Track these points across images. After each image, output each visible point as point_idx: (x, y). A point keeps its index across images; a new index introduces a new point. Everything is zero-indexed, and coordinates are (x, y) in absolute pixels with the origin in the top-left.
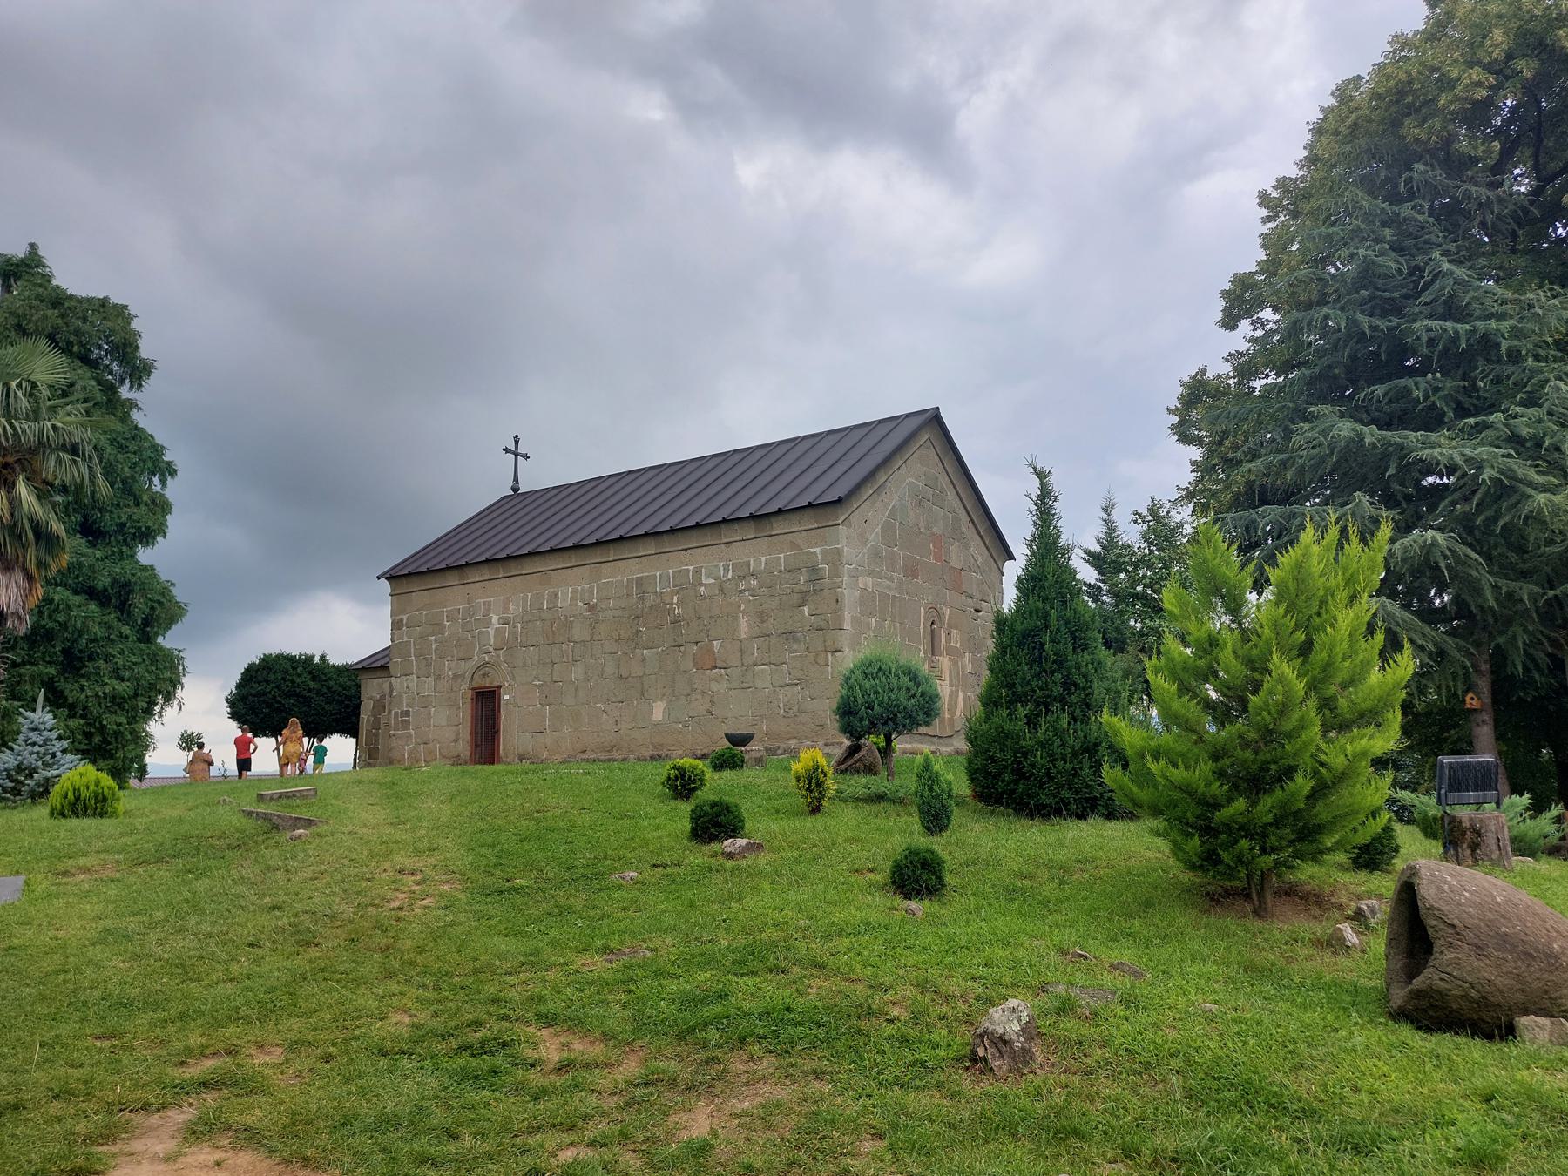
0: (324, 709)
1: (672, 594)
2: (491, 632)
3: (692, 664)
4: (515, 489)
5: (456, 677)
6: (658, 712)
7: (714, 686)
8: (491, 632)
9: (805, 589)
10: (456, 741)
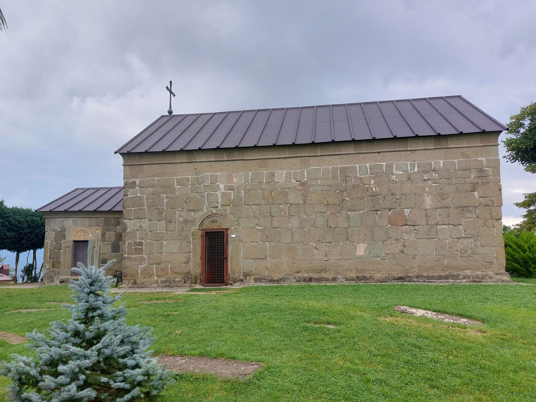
0: (5, 235)
1: (370, 179)
2: (219, 194)
3: (387, 222)
4: (170, 112)
5: (186, 222)
6: (361, 250)
7: (405, 236)
8: (219, 194)
9: (475, 181)
10: (187, 263)
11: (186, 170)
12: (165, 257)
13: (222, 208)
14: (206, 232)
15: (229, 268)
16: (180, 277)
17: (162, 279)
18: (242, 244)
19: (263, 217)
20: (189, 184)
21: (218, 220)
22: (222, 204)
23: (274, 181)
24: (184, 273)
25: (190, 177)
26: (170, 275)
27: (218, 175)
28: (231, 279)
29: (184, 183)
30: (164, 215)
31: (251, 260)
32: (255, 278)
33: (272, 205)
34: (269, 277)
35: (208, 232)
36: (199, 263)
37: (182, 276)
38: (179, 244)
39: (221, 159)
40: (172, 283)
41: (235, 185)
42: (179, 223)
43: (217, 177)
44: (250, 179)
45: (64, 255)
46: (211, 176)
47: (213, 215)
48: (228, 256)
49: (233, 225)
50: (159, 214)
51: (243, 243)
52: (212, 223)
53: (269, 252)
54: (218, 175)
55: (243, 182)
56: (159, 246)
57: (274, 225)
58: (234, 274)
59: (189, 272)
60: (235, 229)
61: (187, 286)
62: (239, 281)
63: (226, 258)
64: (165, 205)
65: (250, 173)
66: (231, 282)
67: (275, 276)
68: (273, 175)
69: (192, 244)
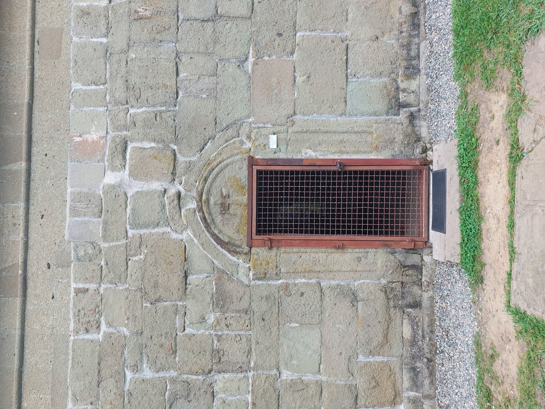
10: (354, 298)
11: (51, 300)
12: (335, 375)
13: (184, 178)
14: (258, 232)
15: (372, 157)
16: (398, 321)
17: (407, 384)
18: (298, 117)
19: (218, 47)
20: (97, 290)
21: (219, 194)
22: (170, 177)
23: (106, 8)
24: (388, 308)
25: (74, 285)
26: (393, 356)
27: (73, 190)
28: (408, 151)
29: (93, 306)
30: (194, 377)
31: (350, 88)
32: (406, 75)
33: (181, 17)
34: (401, 32)
35: (258, 226)
36: (357, 255)
37: (396, 314)
38: (293, 325)
39: (23, 178)
40: (420, 349)
41: (109, 137)
42: (223, 325)
43: (80, 193)
44: (93, 87)
45: (467, 108)
46: (75, 212)
47: (204, 209)
48: (334, 160)
49: (238, 145)
50: (192, 396)
51: (297, 112)
52: (231, 211)
53: (327, 30)
54: (73, 190)
55: (102, 109)
56: (296, 395)
57: (244, 11)
58: (392, 141)
59: (385, 290)
60: (253, 137)
61: (432, 298)
62: (413, 126)
63: (343, 163)
64: (161, 374)
65: (77, 86)
66: (418, 150)
67: (401, 13)
68: (85, 13)
69: (294, 279)
